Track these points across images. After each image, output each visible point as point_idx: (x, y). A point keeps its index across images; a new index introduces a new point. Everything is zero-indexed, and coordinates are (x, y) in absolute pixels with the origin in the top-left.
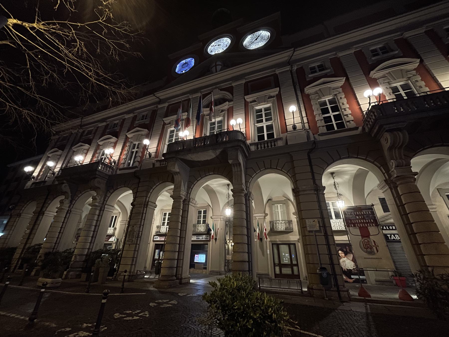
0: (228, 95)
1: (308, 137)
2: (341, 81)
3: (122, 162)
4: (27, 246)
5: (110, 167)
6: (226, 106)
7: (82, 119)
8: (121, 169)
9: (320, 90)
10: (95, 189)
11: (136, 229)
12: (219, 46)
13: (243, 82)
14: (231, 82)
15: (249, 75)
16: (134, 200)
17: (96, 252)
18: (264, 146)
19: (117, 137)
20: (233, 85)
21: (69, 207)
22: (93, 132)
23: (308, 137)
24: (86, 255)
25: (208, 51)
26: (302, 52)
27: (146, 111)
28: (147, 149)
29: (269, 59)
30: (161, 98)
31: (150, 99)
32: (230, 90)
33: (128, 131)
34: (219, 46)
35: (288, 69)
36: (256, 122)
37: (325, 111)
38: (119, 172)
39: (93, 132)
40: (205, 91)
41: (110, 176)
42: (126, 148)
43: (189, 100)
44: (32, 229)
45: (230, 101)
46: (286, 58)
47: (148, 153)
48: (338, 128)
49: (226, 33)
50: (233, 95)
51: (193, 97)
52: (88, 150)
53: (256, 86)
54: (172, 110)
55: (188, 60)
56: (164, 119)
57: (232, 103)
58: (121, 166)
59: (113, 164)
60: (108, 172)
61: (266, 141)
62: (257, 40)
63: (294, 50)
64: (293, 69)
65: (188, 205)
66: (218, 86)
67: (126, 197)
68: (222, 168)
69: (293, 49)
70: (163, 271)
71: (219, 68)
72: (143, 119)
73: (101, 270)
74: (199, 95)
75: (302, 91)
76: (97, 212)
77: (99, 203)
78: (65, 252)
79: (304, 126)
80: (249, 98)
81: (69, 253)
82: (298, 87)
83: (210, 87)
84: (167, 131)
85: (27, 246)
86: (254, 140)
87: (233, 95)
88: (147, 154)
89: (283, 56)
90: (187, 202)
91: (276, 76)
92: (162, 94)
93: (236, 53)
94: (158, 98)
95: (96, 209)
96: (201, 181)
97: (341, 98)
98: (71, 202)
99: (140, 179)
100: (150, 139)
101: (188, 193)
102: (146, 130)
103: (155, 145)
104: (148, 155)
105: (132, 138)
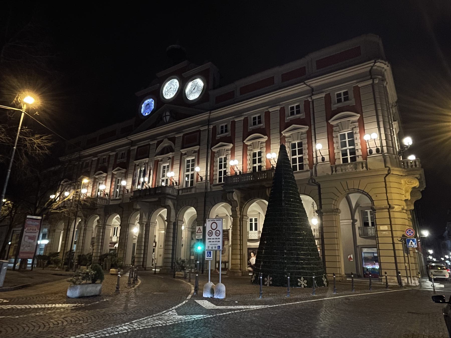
1: (206, 188)
2: (265, 138)
3: (112, 194)
4: (65, 252)
5: (105, 199)
6: (170, 155)
7: (210, 113)
8: (112, 200)
10: (137, 210)
11: (123, 241)
16: (121, 223)
17: (105, 255)
19: (106, 173)
20: (176, 136)
21: (85, 226)
22: (90, 165)
23: (206, 188)
24: (100, 257)
27: (224, 123)
31: (300, 88)
35: (207, 128)
36: (185, 171)
37: (344, 145)
38: (111, 203)
39: (90, 165)
41: (105, 206)
42: (114, 183)
43: (199, 131)
44: (66, 241)
46: (207, 117)
48: (343, 163)
49: (171, 75)
50: (175, 145)
52: (106, 177)
53: (191, 140)
54: (143, 153)
55: (146, 102)
57: (174, 153)
58: (112, 198)
59: (175, 184)
60: (104, 203)
61: (189, 188)
62: (195, 89)
63: (375, 61)
64: (210, 127)
65: (149, 227)
67: (190, 213)
68: (223, 196)
69: (373, 61)
70: (135, 264)
72: (122, 158)
73: (107, 263)
76: (101, 231)
77: (101, 224)
78: (88, 255)
80: (183, 151)
81: (91, 256)
84: (160, 167)
85: (65, 252)
86: (183, 186)
87: (175, 145)
90: (243, 217)
95: (101, 229)
96: (156, 212)
97: (356, 133)
98: (85, 222)
99: (123, 208)
101: (149, 219)
103: (130, 183)
105: (250, 145)
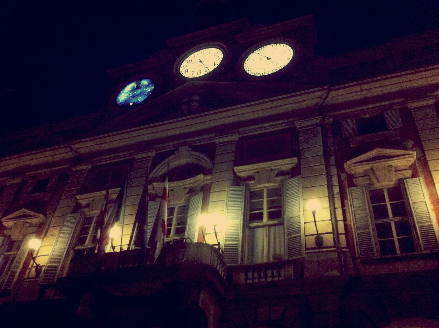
0: (205, 161)
2: (409, 158)
9: (372, 169)
12: (200, 63)
13: (235, 137)
14: (213, 135)
15: (248, 125)
18: (272, 273)
25: (181, 69)
26: (340, 95)
28: (34, 259)
29: (178, 123)
30: (81, 151)
32: (210, 151)
33: (5, 215)
34: (200, 63)
40: (169, 146)
43: (131, 162)
45: (206, 172)
47: (35, 265)
51: (303, 125)
53: (255, 149)
56: (78, 197)
57: (209, 177)
62: (269, 59)
66: (188, 140)
71: (195, 105)
74: (153, 154)
75: (340, 168)
79: (336, 240)
82: (332, 160)
83: (208, 134)
88: (32, 267)
89: (310, 99)
91: (294, 133)
92: (86, 146)
93: (230, 80)
94: (76, 151)
100: (43, 239)
102: (42, 216)
104: (34, 269)
